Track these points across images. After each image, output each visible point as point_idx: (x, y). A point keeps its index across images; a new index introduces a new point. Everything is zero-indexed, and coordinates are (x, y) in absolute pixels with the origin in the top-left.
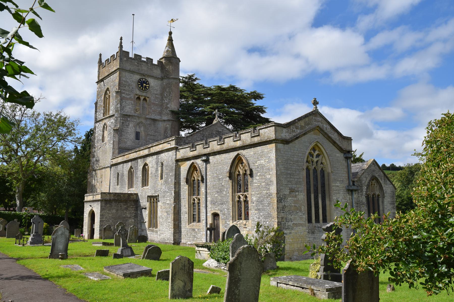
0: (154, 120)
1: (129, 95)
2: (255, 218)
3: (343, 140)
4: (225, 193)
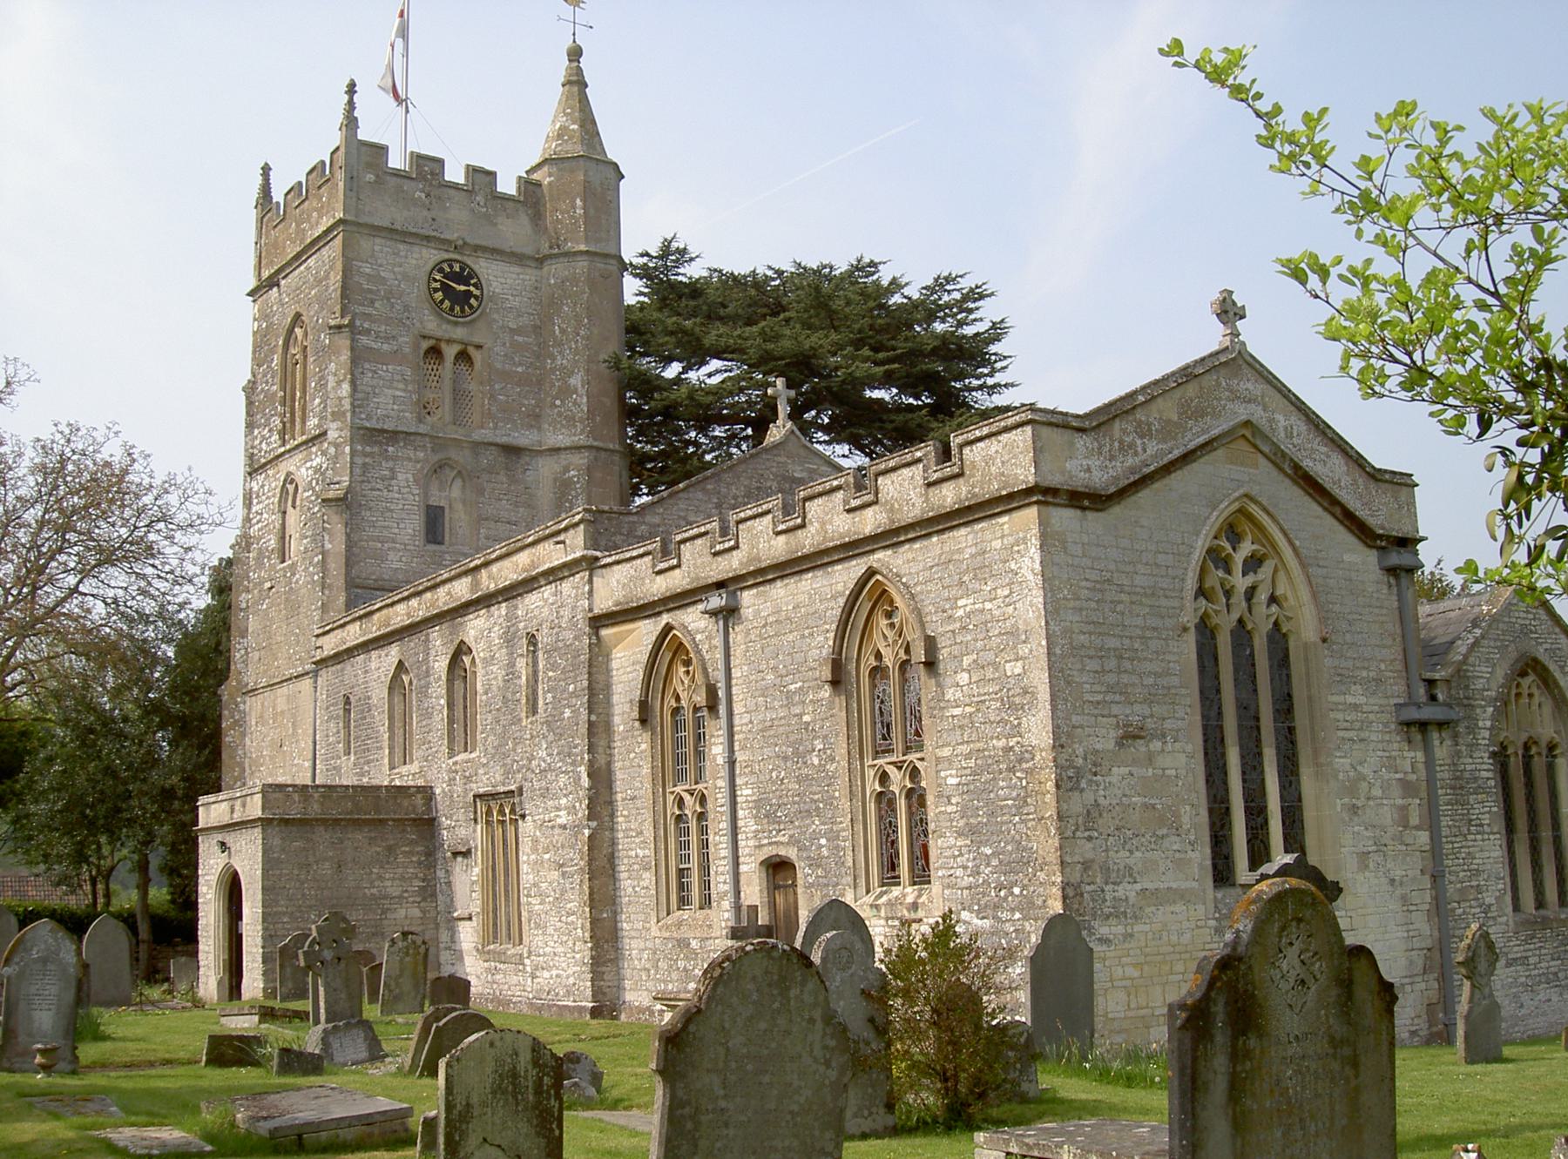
0: (512, 451)
1: (388, 338)
2: (959, 872)
3: (1372, 485)
4: (816, 761)
